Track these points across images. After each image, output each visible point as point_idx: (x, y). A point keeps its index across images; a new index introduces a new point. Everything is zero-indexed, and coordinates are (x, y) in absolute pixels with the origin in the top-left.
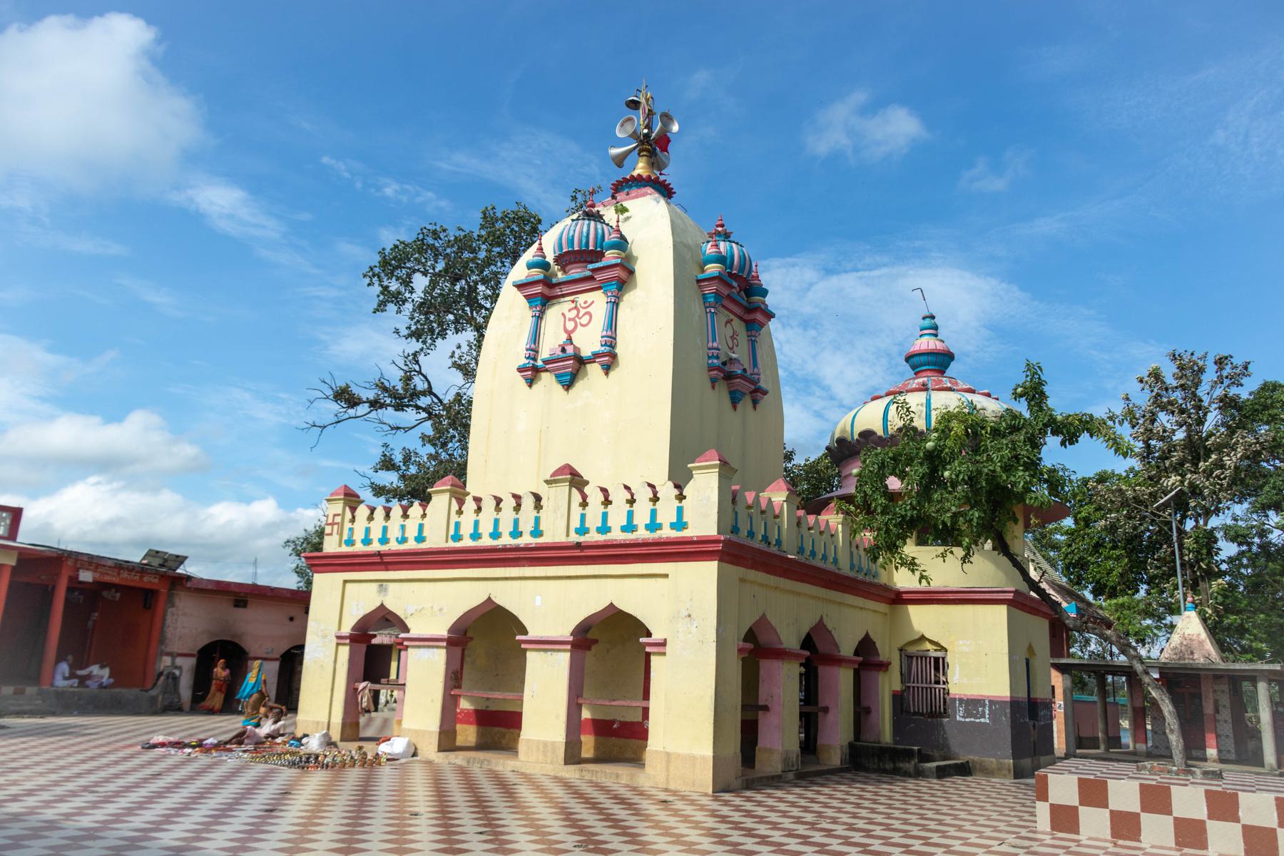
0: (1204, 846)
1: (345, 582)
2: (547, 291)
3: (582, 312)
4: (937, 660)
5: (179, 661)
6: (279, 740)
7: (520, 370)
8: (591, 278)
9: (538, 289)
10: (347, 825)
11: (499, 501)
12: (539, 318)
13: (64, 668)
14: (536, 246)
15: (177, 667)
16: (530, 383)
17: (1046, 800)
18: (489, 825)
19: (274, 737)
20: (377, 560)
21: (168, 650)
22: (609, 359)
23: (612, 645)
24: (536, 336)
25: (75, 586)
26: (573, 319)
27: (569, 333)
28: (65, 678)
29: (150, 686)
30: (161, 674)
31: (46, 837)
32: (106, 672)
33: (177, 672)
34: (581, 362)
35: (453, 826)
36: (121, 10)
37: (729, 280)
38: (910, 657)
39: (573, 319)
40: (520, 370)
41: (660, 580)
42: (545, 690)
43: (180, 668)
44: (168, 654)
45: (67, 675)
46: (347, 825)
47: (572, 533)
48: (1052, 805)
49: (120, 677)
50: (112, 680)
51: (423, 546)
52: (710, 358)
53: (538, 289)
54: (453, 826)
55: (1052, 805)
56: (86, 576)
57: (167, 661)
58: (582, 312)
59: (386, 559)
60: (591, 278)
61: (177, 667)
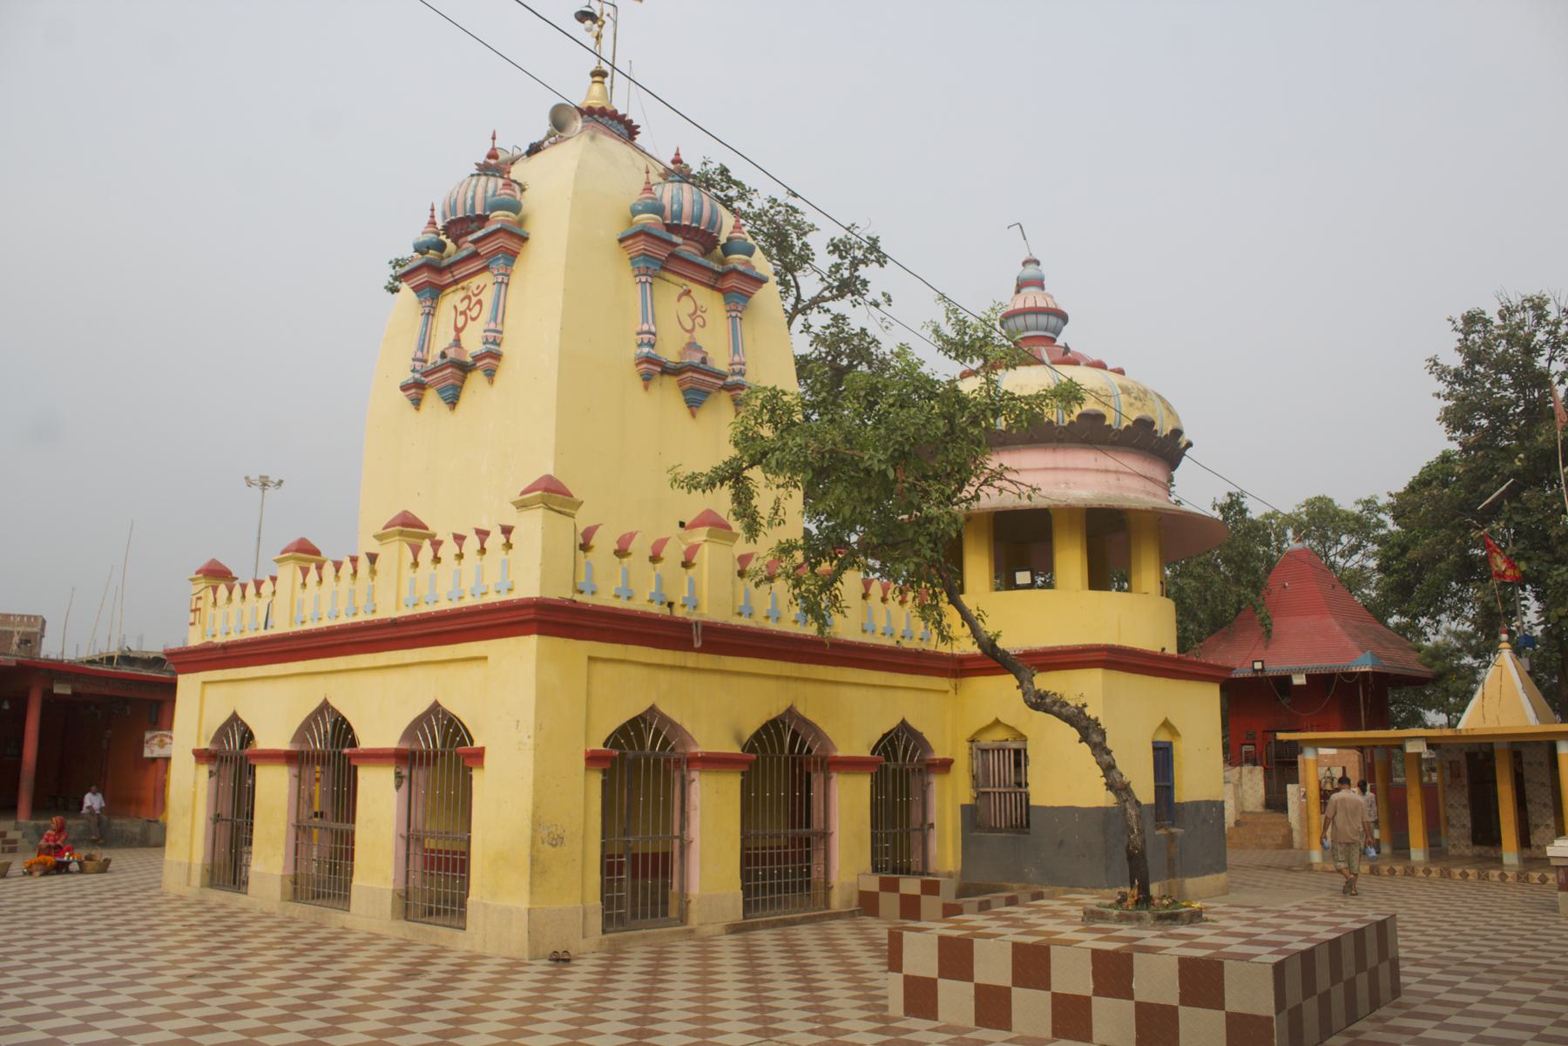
0: (1088, 1038)
1: (204, 683)
2: (436, 279)
3: (474, 300)
4: (1017, 752)
7: (404, 388)
8: (474, 255)
9: (423, 277)
10: (660, 990)
11: (354, 560)
12: (430, 315)
16: (417, 402)
17: (900, 970)
18: (811, 989)
20: (221, 654)
22: (490, 360)
23: (441, 755)
24: (424, 342)
25: (51, 705)
26: (463, 313)
27: (458, 330)
31: (377, 1008)
34: (464, 368)
35: (766, 990)
37: (666, 235)
38: (985, 751)
39: (463, 313)
40: (404, 388)
41: (474, 666)
42: (848, 804)
46: (660, 990)
47: (402, 606)
48: (906, 978)
51: (270, 632)
52: (640, 345)
53: (423, 277)
54: (766, 990)
55: (906, 978)
56: (62, 689)
58: (474, 300)
59: (234, 652)
60: (474, 255)
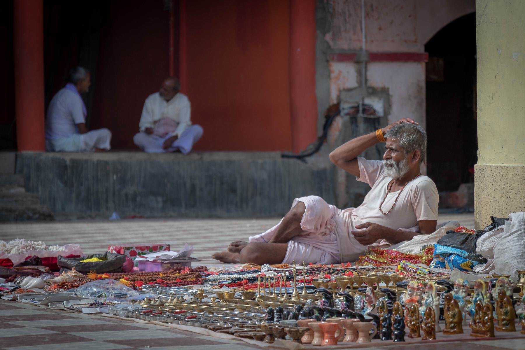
5: (379, 74)
6: (414, 246)
13: (71, 103)
14: (32, 289)
15: (373, 92)
19: (395, 237)
21: (344, 44)
28: (81, 129)
29: (306, 144)
30: (333, 111)
32: (181, 107)
33: (378, 106)
36: (146, 96)
43: (383, 93)
44: (347, 57)
45: (80, 119)
49: (219, 126)
50: (198, 130)
57: (344, 75)
61: (373, 92)
